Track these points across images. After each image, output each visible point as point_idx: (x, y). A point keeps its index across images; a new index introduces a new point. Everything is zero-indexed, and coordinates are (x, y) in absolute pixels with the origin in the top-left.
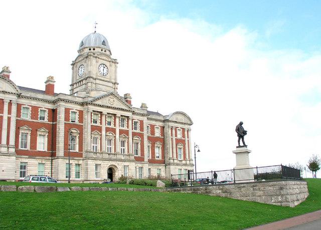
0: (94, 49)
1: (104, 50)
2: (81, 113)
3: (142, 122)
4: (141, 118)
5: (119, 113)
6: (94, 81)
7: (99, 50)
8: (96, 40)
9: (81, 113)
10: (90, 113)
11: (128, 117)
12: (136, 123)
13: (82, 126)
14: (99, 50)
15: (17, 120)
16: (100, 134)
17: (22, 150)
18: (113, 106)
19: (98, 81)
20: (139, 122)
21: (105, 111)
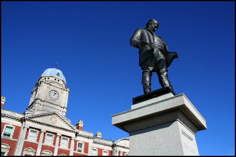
0: (48, 78)
1: (57, 80)
2: (18, 129)
3: (87, 145)
4: (87, 140)
5: (60, 132)
6: (42, 103)
7: (53, 79)
8: (122, 126)
9: (18, 129)
10: (26, 129)
11: (70, 137)
12: (80, 145)
13: (16, 142)
14: (53, 79)
15: (7, 134)
16: (35, 151)
17: (62, 153)
18: (53, 125)
19: (45, 103)
20: (84, 143)
21: (44, 128)
